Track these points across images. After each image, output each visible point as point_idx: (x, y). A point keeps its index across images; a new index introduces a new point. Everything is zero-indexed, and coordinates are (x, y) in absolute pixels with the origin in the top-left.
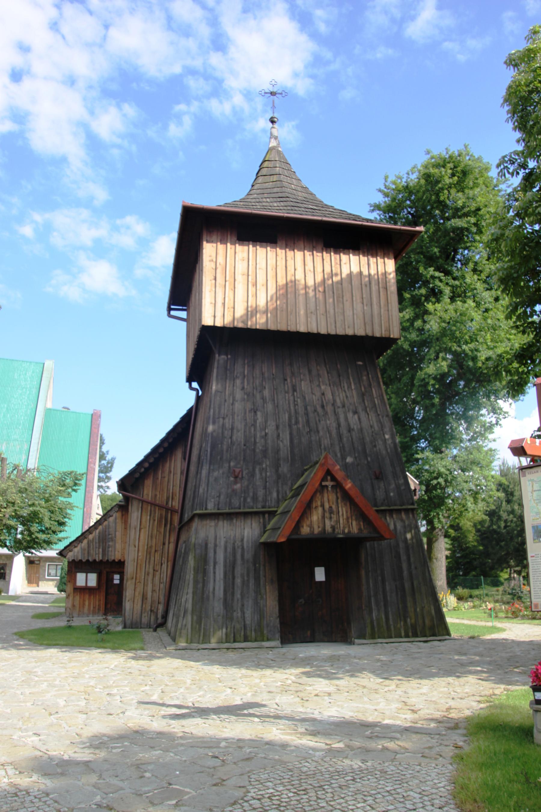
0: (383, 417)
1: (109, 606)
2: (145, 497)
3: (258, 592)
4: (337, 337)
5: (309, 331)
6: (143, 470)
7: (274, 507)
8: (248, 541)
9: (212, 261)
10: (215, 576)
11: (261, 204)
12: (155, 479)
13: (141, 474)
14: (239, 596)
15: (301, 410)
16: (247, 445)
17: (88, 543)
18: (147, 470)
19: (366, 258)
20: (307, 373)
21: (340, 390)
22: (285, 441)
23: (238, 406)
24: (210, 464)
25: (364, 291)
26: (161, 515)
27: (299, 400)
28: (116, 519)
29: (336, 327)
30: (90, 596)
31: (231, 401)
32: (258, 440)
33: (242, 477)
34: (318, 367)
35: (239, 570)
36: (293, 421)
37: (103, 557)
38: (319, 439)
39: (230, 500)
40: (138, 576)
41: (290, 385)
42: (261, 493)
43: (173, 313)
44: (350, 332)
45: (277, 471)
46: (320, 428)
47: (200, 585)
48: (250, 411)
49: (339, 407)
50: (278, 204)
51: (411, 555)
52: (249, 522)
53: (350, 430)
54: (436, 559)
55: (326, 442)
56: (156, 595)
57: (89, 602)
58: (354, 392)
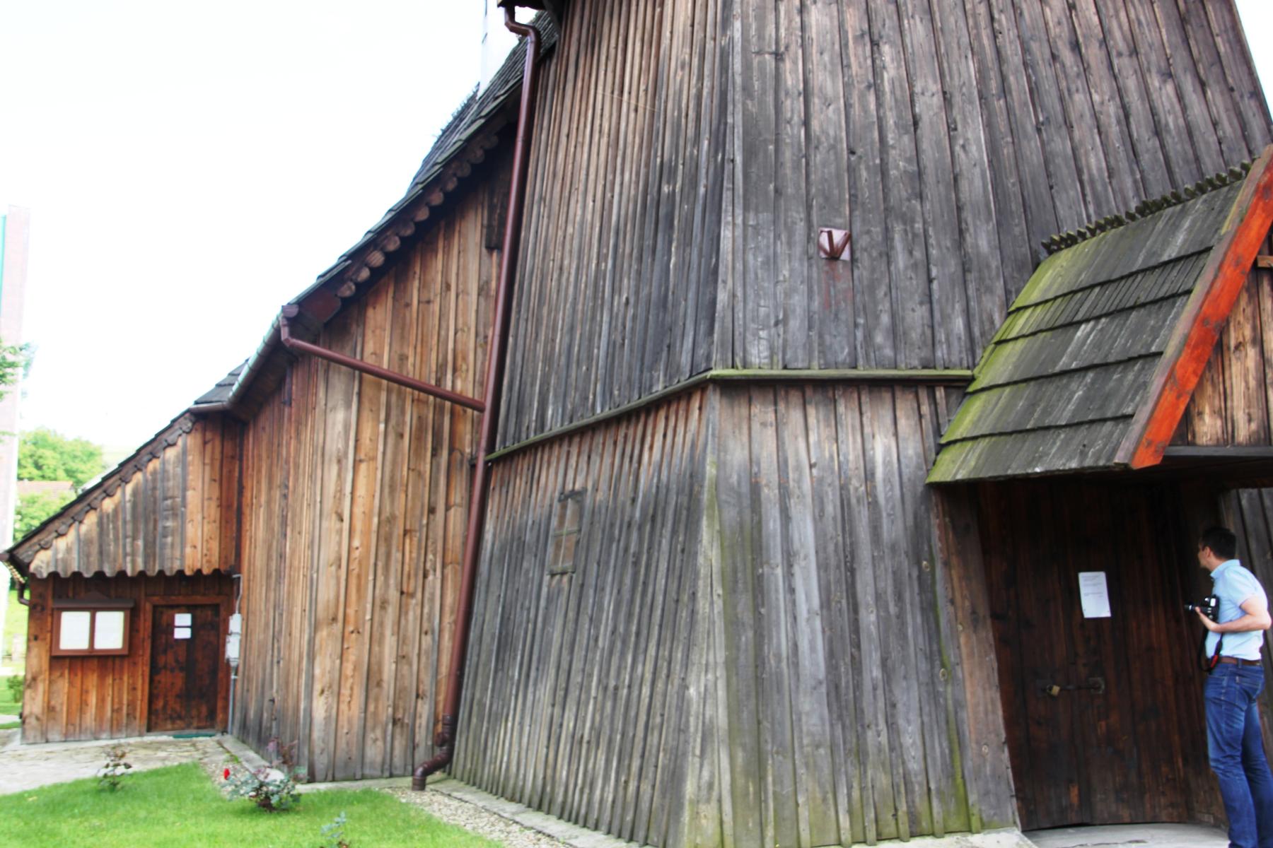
1: (160, 704)
2: (369, 360)
3: (935, 655)
6: (365, 274)
8: (887, 480)
12: (401, 305)
14: (877, 673)
16: (860, 151)
17: (100, 523)
18: (377, 273)
24: (746, 209)
28: (185, 452)
30: (102, 678)
32: (891, 138)
36: (994, 85)
37: (146, 563)
40: (351, 612)
47: (747, 636)
49: (1120, 55)
53: (1158, 131)
56: (410, 672)
57: (97, 695)
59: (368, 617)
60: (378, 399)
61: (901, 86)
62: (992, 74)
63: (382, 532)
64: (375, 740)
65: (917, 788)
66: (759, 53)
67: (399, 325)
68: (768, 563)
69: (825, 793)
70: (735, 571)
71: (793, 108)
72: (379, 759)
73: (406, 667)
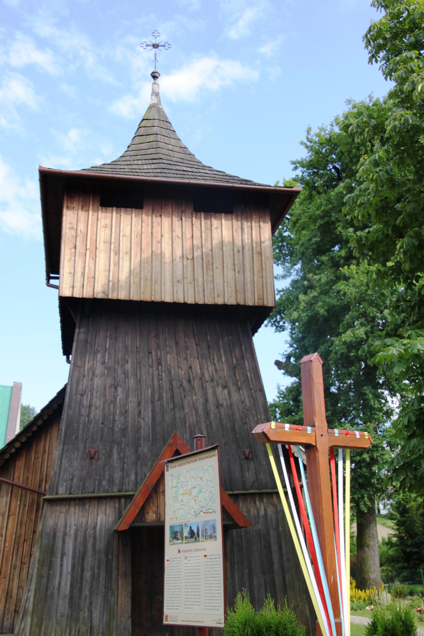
0: (255, 391)
2: (16, 482)
3: (108, 588)
4: (205, 307)
5: (175, 300)
6: (13, 450)
7: (132, 491)
8: (101, 529)
9: (73, 228)
10: (61, 570)
11: (130, 167)
13: (11, 454)
14: (87, 593)
15: (165, 384)
19: (239, 223)
20: (174, 345)
21: (209, 363)
22: (146, 419)
23: (97, 381)
24: (64, 444)
25: (236, 257)
26: (33, 500)
27: (164, 374)
29: (204, 296)
31: (90, 377)
32: (117, 418)
33: (99, 458)
34: (186, 339)
35: (89, 562)
36: (156, 397)
38: (184, 416)
39: (84, 483)
41: (154, 358)
42: (117, 475)
43: (52, 282)
44: (220, 301)
45: (136, 451)
46: (186, 404)
47: (44, 581)
48: (110, 387)
49: (207, 382)
50: (149, 166)
51: (283, 545)
52: (103, 507)
53: (218, 406)
54: (368, 546)
55: (191, 419)
58: (225, 365)
59: (9, 572)
60: (18, 493)
61: (123, 400)
62: (157, 393)
63: (16, 541)
64: (8, 619)
65: (95, 631)
66: (76, 395)
67: (27, 466)
68: (55, 557)
69: (62, 632)
70: (44, 560)
71: (84, 411)
72: (8, 626)
73: (21, 591)
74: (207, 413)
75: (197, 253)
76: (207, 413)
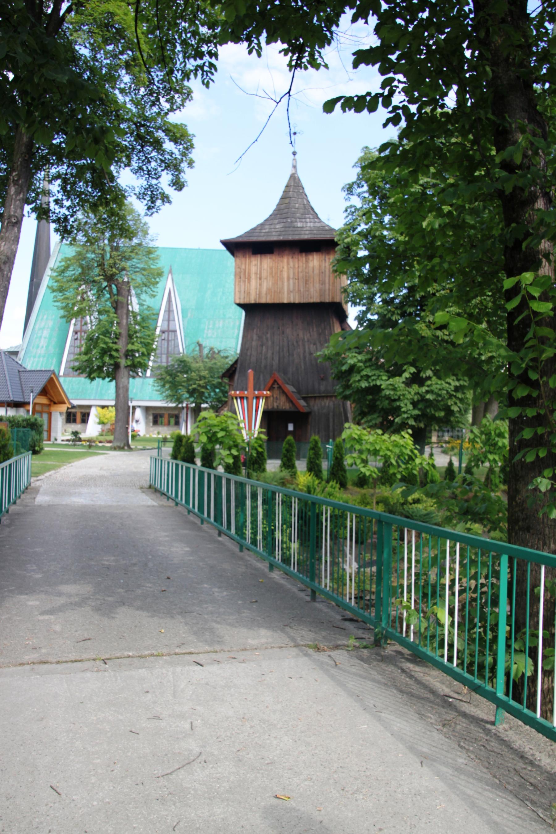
23: (254, 343)
74: (305, 357)
75: (301, 275)
76: (305, 357)
